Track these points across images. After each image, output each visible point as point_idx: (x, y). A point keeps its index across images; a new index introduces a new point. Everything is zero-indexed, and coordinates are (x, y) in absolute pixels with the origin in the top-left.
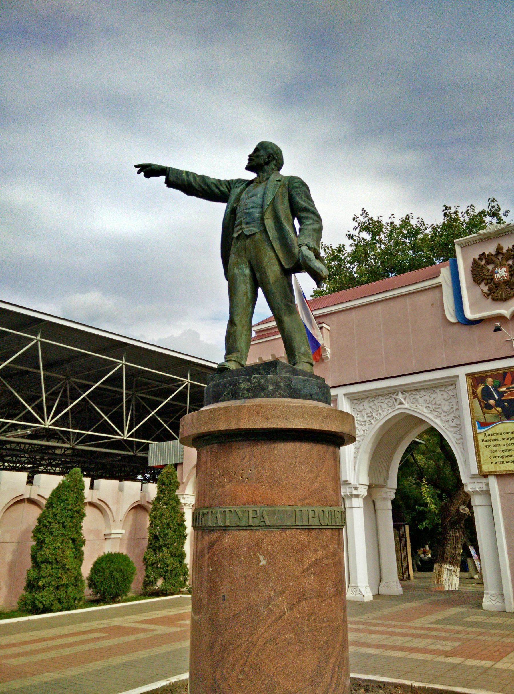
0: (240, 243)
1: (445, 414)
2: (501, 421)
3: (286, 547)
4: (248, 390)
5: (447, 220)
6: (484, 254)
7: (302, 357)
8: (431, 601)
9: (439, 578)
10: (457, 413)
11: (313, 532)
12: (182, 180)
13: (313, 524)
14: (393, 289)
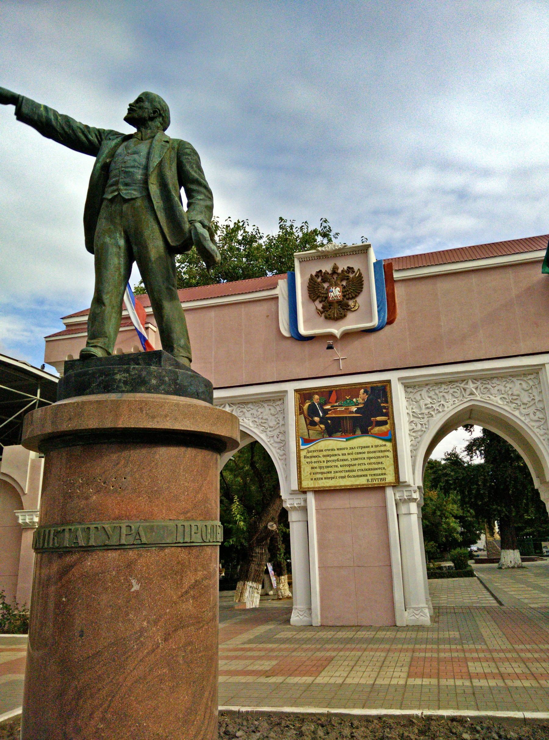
0: (115, 207)
1: (524, 406)
2: (323, 438)
3: (164, 569)
4: (125, 383)
5: (283, 233)
6: (321, 271)
7: (181, 350)
8: (238, 621)
9: (241, 596)
10: (282, 429)
11: (195, 550)
12: (39, 115)
13: (195, 541)
14: (228, 296)
